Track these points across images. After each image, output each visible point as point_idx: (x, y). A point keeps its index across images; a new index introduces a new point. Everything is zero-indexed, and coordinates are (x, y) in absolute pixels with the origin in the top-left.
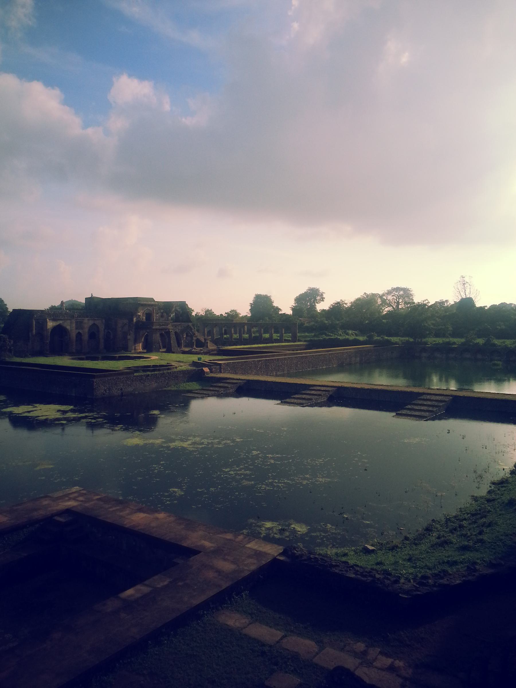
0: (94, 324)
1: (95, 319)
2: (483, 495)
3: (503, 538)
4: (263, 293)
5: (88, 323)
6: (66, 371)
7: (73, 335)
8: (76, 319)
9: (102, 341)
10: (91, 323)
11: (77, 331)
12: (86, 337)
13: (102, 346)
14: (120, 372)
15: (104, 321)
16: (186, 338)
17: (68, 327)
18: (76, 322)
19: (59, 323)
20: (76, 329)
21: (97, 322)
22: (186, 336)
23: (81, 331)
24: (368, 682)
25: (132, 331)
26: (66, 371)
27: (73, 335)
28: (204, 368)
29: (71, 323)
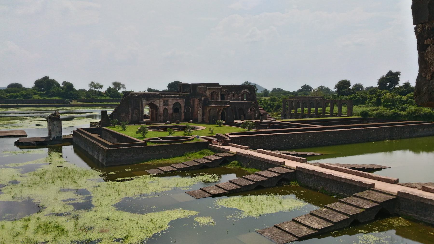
0: (177, 103)
1: (178, 99)
2: (183, 167)
3: (405, 105)
4: (90, 82)
5: (172, 102)
6: (132, 147)
7: (161, 110)
8: (163, 99)
9: (183, 114)
10: (175, 101)
11: (164, 107)
12: (171, 111)
13: (183, 118)
14: (88, 138)
15: (184, 100)
16: (250, 112)
17: (158, 105)
18: (163, 101)
19: (151, 102)
20: (164, 105)
21: (178, 101)
22: (250, 111)
23: (167, 107)
24: (320, 229)
25: (201, 108)
26: (132, 147)
27: (161, 110)
28: (225, 121)
29: (160, 102)
